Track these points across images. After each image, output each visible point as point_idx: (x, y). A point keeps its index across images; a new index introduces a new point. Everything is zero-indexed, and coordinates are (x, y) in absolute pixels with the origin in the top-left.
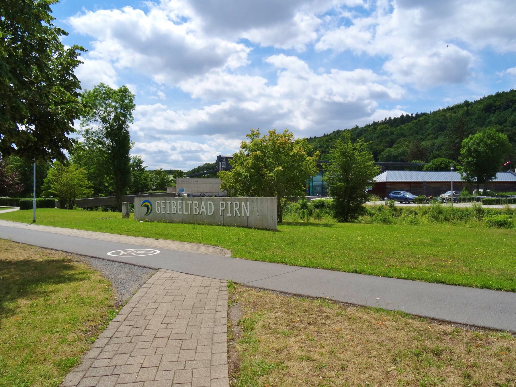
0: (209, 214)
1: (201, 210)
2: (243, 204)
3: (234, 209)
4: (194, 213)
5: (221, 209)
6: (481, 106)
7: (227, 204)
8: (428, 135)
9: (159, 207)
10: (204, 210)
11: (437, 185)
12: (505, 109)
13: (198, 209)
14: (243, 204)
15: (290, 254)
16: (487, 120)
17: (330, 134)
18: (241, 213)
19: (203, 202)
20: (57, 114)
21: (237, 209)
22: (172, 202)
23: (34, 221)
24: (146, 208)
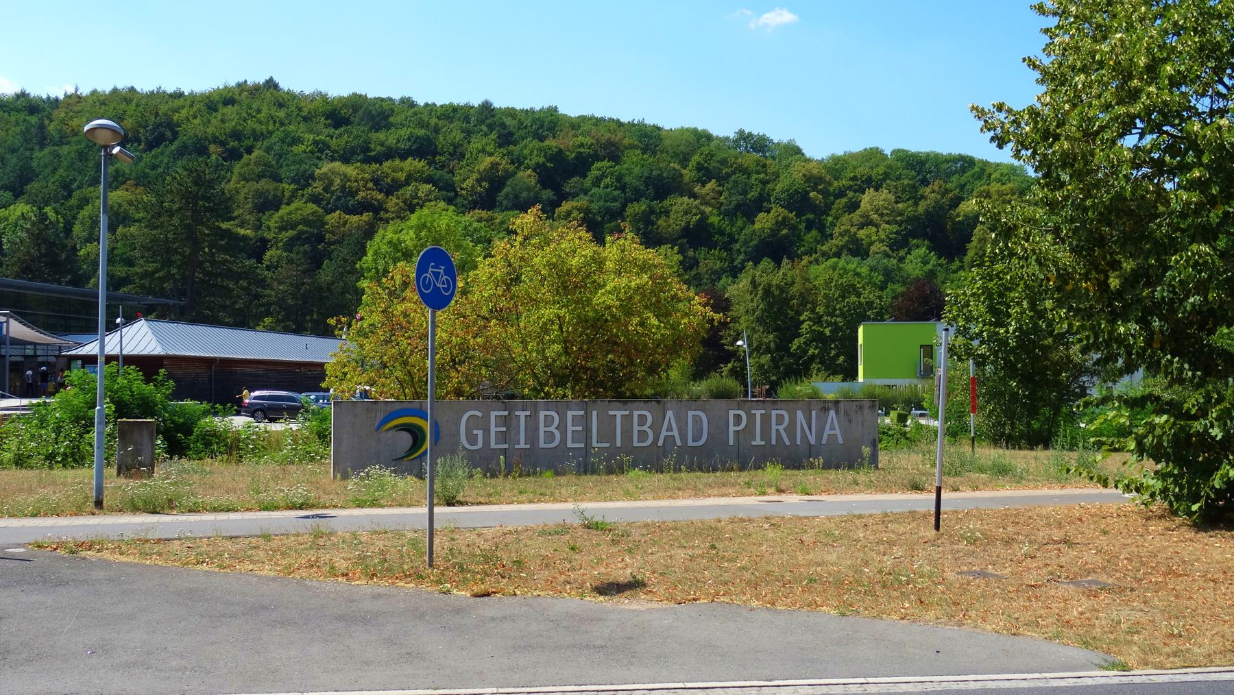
0: (690, 444)
1: (664, 433)
2: (800, 414)
3: (774, 427)
4: (636, 444)
5: (732, 428)
7: (751, 418)
9: (480, 433)
10: (675, 433)
11: (252, 370)
12: (150, 147)
13: (557, 433)
14: (800, 414)
15: (561, 574)
18: (792, 436)
19: (670, 414)
20: (1193, 305)
21: (781, 428)
22: (542, 414)
23: (99, 504)
24: (406, 438)
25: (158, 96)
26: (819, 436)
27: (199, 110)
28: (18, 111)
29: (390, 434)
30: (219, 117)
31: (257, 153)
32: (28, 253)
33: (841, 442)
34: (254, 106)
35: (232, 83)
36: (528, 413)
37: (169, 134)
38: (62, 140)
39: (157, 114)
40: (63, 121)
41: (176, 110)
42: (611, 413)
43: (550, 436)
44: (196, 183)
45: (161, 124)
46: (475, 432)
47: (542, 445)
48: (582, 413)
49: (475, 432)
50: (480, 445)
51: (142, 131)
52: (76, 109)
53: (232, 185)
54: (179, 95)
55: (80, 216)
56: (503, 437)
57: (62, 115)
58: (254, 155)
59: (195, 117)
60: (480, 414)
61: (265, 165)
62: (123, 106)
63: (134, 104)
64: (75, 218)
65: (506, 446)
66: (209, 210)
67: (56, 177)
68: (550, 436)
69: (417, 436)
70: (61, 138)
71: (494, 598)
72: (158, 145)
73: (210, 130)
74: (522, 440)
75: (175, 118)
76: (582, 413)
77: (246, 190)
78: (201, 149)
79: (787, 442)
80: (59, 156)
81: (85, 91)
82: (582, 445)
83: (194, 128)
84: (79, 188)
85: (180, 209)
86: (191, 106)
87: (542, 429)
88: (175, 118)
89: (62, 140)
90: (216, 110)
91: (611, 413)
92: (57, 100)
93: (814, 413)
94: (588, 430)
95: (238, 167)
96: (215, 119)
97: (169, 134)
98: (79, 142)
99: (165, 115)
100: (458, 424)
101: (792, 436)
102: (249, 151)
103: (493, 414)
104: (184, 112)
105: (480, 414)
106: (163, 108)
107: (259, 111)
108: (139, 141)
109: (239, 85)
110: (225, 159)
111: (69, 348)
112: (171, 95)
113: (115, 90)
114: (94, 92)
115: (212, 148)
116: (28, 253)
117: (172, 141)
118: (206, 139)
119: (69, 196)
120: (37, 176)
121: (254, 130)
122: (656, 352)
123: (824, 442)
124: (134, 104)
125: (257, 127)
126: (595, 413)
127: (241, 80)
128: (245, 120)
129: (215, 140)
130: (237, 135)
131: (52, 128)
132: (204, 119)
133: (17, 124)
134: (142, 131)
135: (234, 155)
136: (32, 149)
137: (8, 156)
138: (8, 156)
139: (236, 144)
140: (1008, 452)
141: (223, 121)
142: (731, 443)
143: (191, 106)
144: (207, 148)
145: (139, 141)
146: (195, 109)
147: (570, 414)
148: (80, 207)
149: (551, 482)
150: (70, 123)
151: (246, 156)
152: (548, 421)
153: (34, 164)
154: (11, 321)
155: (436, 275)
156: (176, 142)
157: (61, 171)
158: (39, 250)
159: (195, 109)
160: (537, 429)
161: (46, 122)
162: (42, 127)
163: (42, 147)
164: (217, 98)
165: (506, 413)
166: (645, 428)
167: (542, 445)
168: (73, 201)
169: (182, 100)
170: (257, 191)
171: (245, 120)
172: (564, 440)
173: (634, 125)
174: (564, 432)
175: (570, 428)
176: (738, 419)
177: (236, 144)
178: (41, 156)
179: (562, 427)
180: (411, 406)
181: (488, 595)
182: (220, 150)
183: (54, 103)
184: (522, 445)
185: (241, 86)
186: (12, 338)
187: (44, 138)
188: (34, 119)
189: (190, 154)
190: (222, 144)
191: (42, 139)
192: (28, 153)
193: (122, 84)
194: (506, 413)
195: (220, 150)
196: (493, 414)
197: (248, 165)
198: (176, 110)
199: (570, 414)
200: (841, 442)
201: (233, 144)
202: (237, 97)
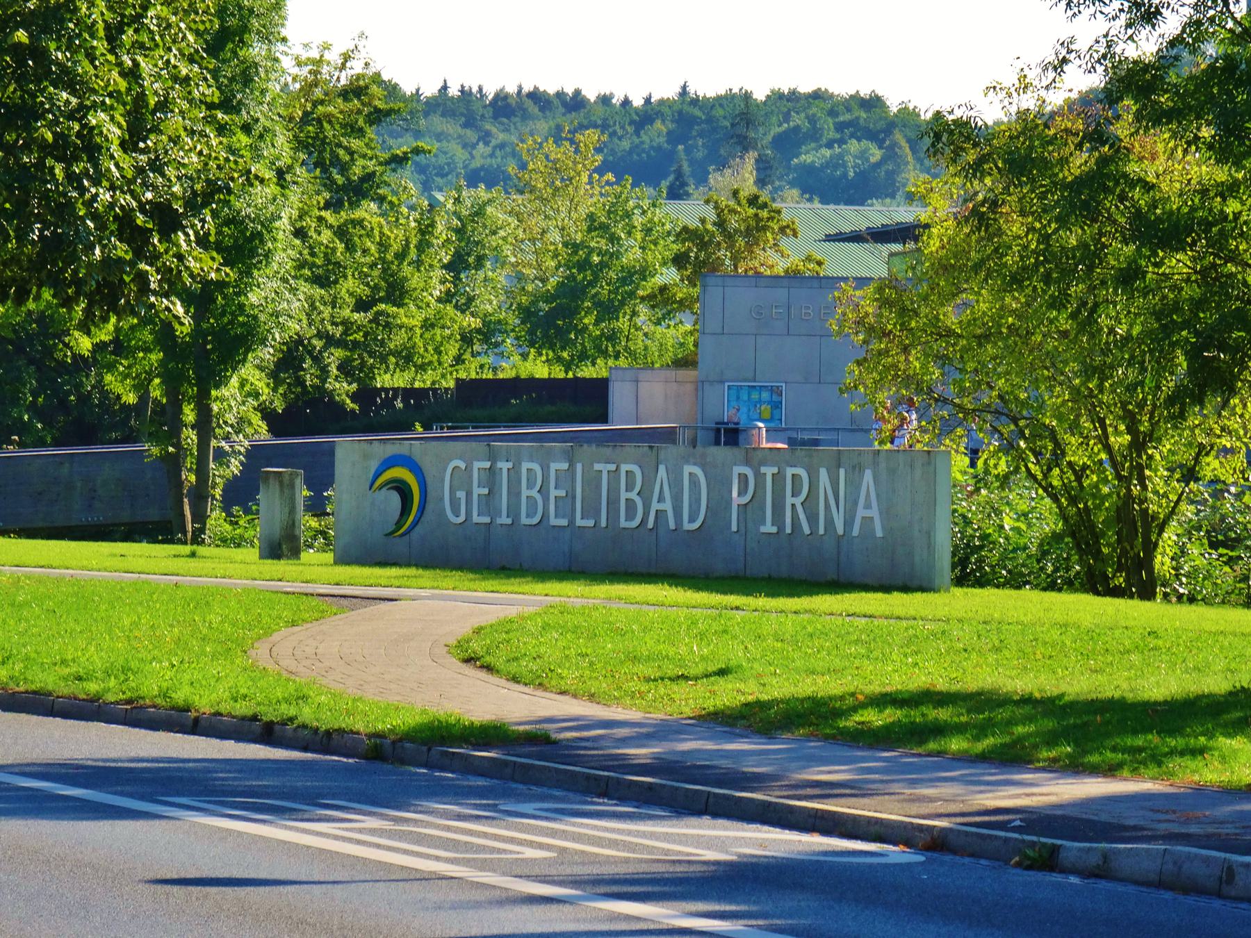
2: (823, 473)
7: (760, 477)
13: (538, 497)
14: (823, 473)
18: (813, 519)
22: (525, 466)
24: (395, 499)
26: (848, 523)
33: (879, 534)
71: (151, 876)
79: (807, 530)
93: (842, 471)
101: (813, 519)
122: (141, 320)
123: (856, 532)
140: (1064, 688)
142: (734, 528)
160: (519, 493)
173: (734, 96)
176: (743, 479)
200: (879, 534)
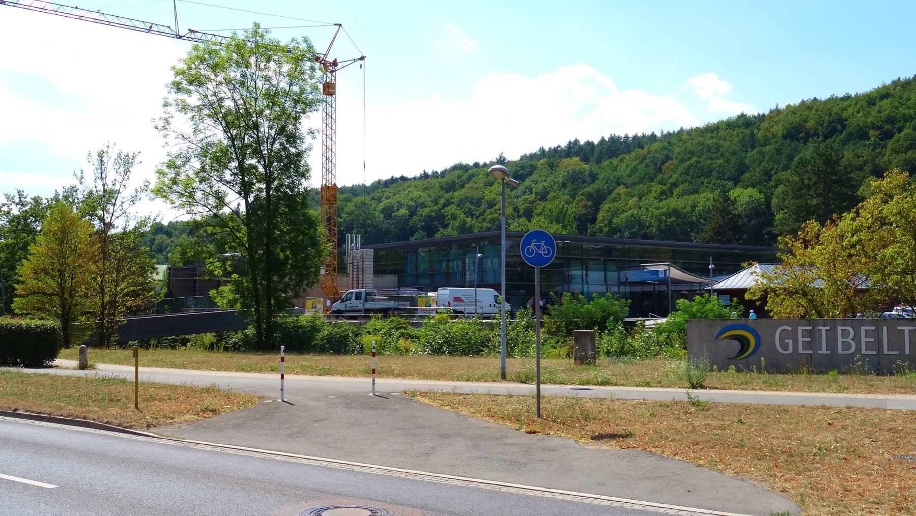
6: (778, 129)
8: (675, 185)
9: (790, 342)
12: (826, 137)
16: (798, 157)
17: (444, 173)
22: (840, 329)
24: (736, 345)
25: (833, 100)
27: (862, 106)
28: (739, 127)
29: (725, 341)
30: (877, 109)
31: (905, 131)
32: (717, 222)
34: (905, 96)
35: (888, 82)
36: (828, 328)
37: (839, 127)
38: (766, 142)
39: (830, 114)
40: (767, 130)
41: (845, 109)
42: (899, 328)
43: (847, 346)
44: (825, 164)
45: (833, 121)
46: (786, 341)
47: (840, 351)
48: (874, 328)
49: (786, 341)
50: (790, 350)
51: (820, 128)
52: (776, 119)
53: (886, 158)
54: (847, 98)
55: (776, 193)
56: (808, 345)
57: (767, 125)
58: (903, 133)
59: (858, 112)
60: (790, 329)
61: (912, 140)
62: (807, 113)
63: (814, 110)
64: (772, 194)
65: (811, 352)
66: (836, 181)
67: (761, 168)
68: (847, 346)
69: (744, 343)
70: (765, 141)
72: (831, 137)
73: (869, 120)
74: (824, 348)
75: (844, 115)
76: (874, 328)
77: (897, 160)
78: (863, 135)
80: (763, 154)
81: (782, 106)
82: (875, 353)
83: (857, 120)
84: (776, 173)
85: (815, 184)
86: (856, 104)
87: (840, 340)
88: (844, 115)
89: (766, 142)
90: (875, 104)
91: (899, 328)
92: (764, 115)
94: (879, 342)
95: (890, 144)
96: (874, 111)
97: (839, 127)
98: (777, 142)
99: (836, 114)
100: (773, 335)
102: (900, 130)
103: (800, 329)
104: (850, 110)
105: (790, 329)
106: (835, 109)
107: (909, 99)
108: (818, 135)
109: (894, 82)
110: (881, 140)
111: (707, 285)
112: (842, 99)
113: (803, 102)
114: (788, 106)
115: (872, 132)
116: (717, 222)
117: (841, 132)
118: (867, 126)
119: (770, 179)
120: (748, 169)
121: (904, 114)
124: (814, 110)
125: (907, 112)
126: (885, 329)
127: (896, 78)
128: (897, 108)
129: (874, 127)
130: (891, 120)
131: (760, 135)
132: (866, 112)
133: (738, 136)
134: (820, 128)
135: (888, 135)
136: (747, 151)
137: (731, 158)
138: (731, 158)
139: (890, 127)
141: (880, 112)
143: (856, 104)
144: (867, 133)
145: (818, 135)
146: (858, 106)
147: (863, 329)
148: (776, 186)
149: (875, 377)
150: (771, 130)
151: (896, 135)
152: (845, 334)
153: (747, 161)
154: (672, 268)
155: (539, 247)
156: (845, 132)
157: (764, 164)
158: (724, 220)
159: (858, 106)
161: (756, 131)
162: (752, 135)
163: (753, 148)
164: (875, 95)
165: (810, 328)
166: (849, 340)
167: (840, 351)
168: (772, 183)
169: (849, 101)
170: (905, 160)
171: (897, 108)
172: (858, 349)
174: (858, 343)
175: (864, 340)
177: (890, 127)
178: (752, 154)
179: (857, 338)
180: (739, 322)
181: (535, 433)
182: (877, 133)
183: (762, 118)
184: (824, 351)
185: (895, 83)
186: (672, 279)
187: (754, 142)
188: (747, 131)
189: (854, 139)
190: (879, 128)
191: (753, 142)
192: (744, 154)
193: (808, 96)
194: (810, 328)
195: (877, 133)
196: (800, 329)
197: (897, 142)
198: (845, 109)
199: (863, 329)
201: (888, 127)
202: (892, 92)
